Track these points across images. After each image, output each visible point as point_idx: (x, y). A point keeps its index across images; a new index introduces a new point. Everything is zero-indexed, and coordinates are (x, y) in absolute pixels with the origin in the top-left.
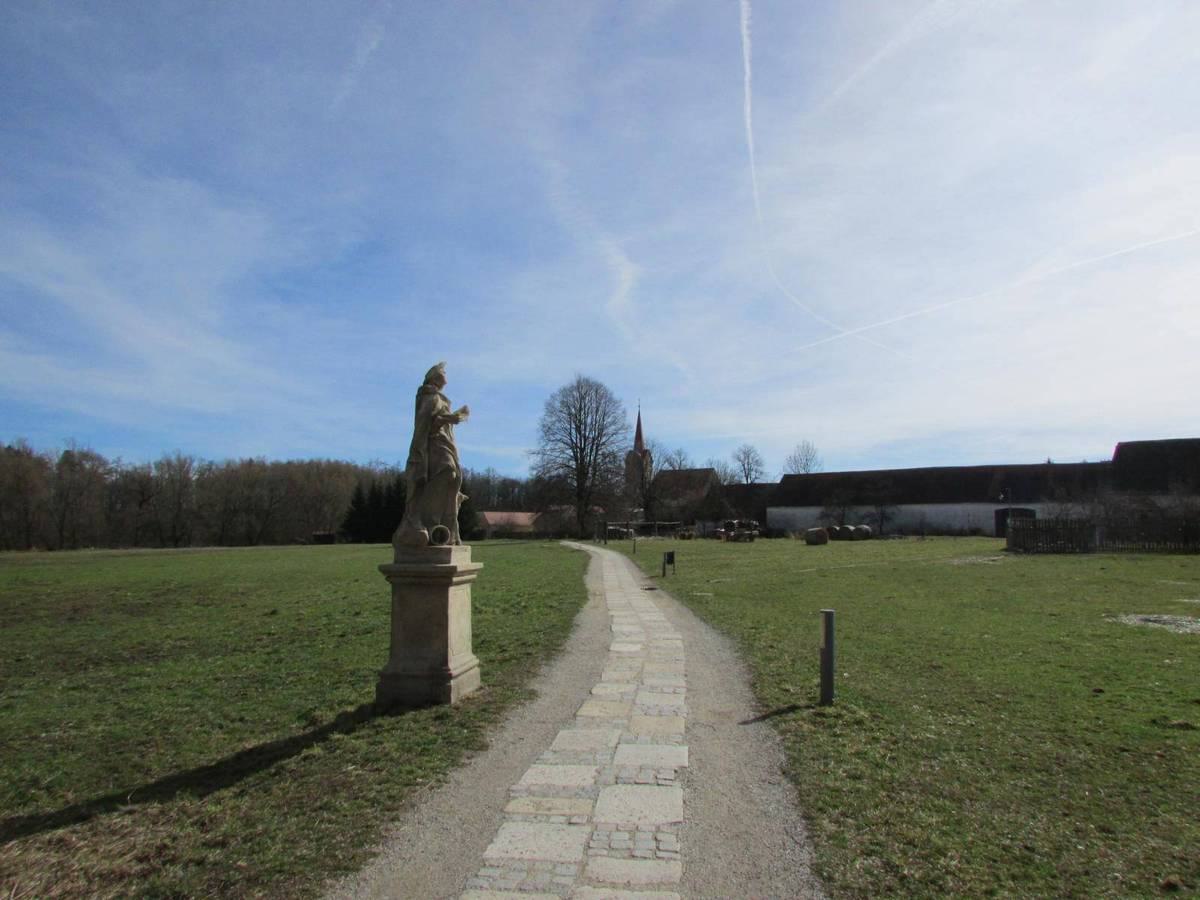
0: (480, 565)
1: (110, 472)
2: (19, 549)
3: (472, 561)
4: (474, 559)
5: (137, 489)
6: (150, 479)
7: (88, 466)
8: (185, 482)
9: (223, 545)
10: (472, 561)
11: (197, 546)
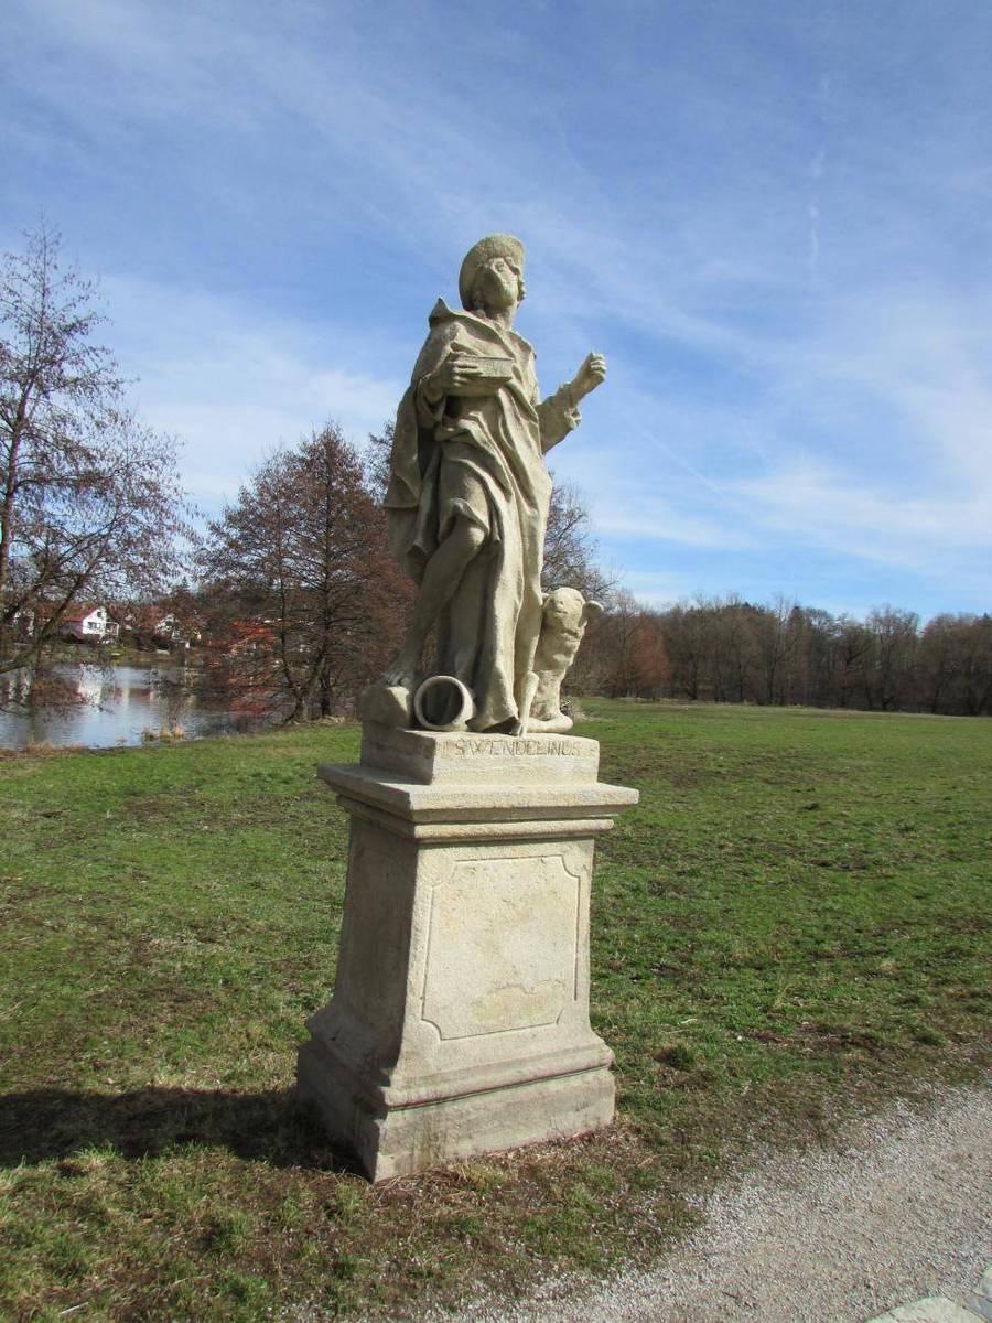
0: (627, 795)
1: (835, 628)
2: (733, 701)
3: (602, 777)
4: (610, 771)
5: (855, 644)
6: (862, 631)
7: (815, 623)
8: (910, 639)
9: (937, 713)
10: (602, 777)
11: (704, 700)
